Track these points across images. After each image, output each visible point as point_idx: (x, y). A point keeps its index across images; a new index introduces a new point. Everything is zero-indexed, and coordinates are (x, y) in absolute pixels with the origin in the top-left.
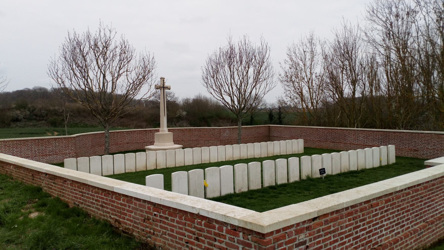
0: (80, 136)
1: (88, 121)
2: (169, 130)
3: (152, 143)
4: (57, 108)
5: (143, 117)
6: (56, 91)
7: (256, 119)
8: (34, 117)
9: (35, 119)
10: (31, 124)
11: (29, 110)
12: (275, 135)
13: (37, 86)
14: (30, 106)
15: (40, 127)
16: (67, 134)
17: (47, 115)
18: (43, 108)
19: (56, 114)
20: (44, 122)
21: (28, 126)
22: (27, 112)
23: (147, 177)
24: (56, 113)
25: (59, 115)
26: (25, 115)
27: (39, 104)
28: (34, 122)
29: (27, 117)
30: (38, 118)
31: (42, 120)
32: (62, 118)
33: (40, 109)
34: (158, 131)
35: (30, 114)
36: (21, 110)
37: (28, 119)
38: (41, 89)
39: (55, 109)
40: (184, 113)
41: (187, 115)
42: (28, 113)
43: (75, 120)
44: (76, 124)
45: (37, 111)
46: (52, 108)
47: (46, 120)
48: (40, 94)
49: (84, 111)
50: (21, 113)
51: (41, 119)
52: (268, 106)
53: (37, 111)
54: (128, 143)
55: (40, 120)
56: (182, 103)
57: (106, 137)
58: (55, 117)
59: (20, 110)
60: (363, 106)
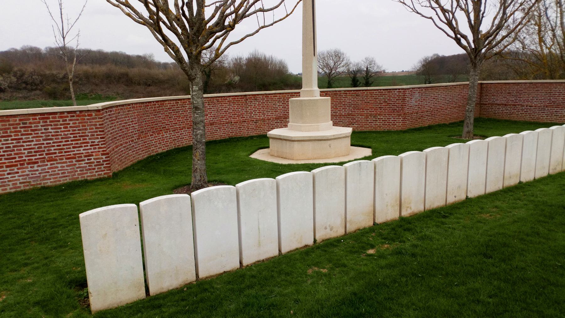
0: (111, 107)
1: (102, 90)
2: (322, 94)
3: (283, 121)
4: (55, 72)
5: (178, 84)
6: (52, 52)
7: (371, 80)
8: (24, 85)
9: (25, 88)
10: (21, 95)
11: (15, 76)
12: (498, 102)
13: (26, 45)
14: (16, 69)
15: (34, 99)
16: (75, 103)
17: (41, 82)
18: (35, 72)
19: (54, 81)
20: (38, 92)
21: (16, 99)
22: (13, 78)
23: (81, 215)
24: (54, 79)
25: (59, 83)
26: (11, 83)
27: (30, 68)
28: (24, 93)
29: (13, 85)
30: (29, 87)
31: (36, 89)
32: (63, 86)
33: (32, 74)
34: (298, 95)
35: (17, 81)
36: (4, 75)
37: (15, 88)
38: (32, 49)
39: (53, 74)
40: (237, 78)
41: (241, 80)
42: (14, 79)
43: (84, 89)
44: (85, 95)
45: (26, 76)
46: (48, 72)
47: (40, 90)
48: (31, 55)
49: (95, 77)
50: (4, 80)
51: (34, 88)
52: (352, 68)
53: (26, 76)
54: (211, 124)
55: (32, 90)
56: (232, 65)
57: (196, 108)
58: (54, 85)
59: (2, 76)
60: (549, 58)
